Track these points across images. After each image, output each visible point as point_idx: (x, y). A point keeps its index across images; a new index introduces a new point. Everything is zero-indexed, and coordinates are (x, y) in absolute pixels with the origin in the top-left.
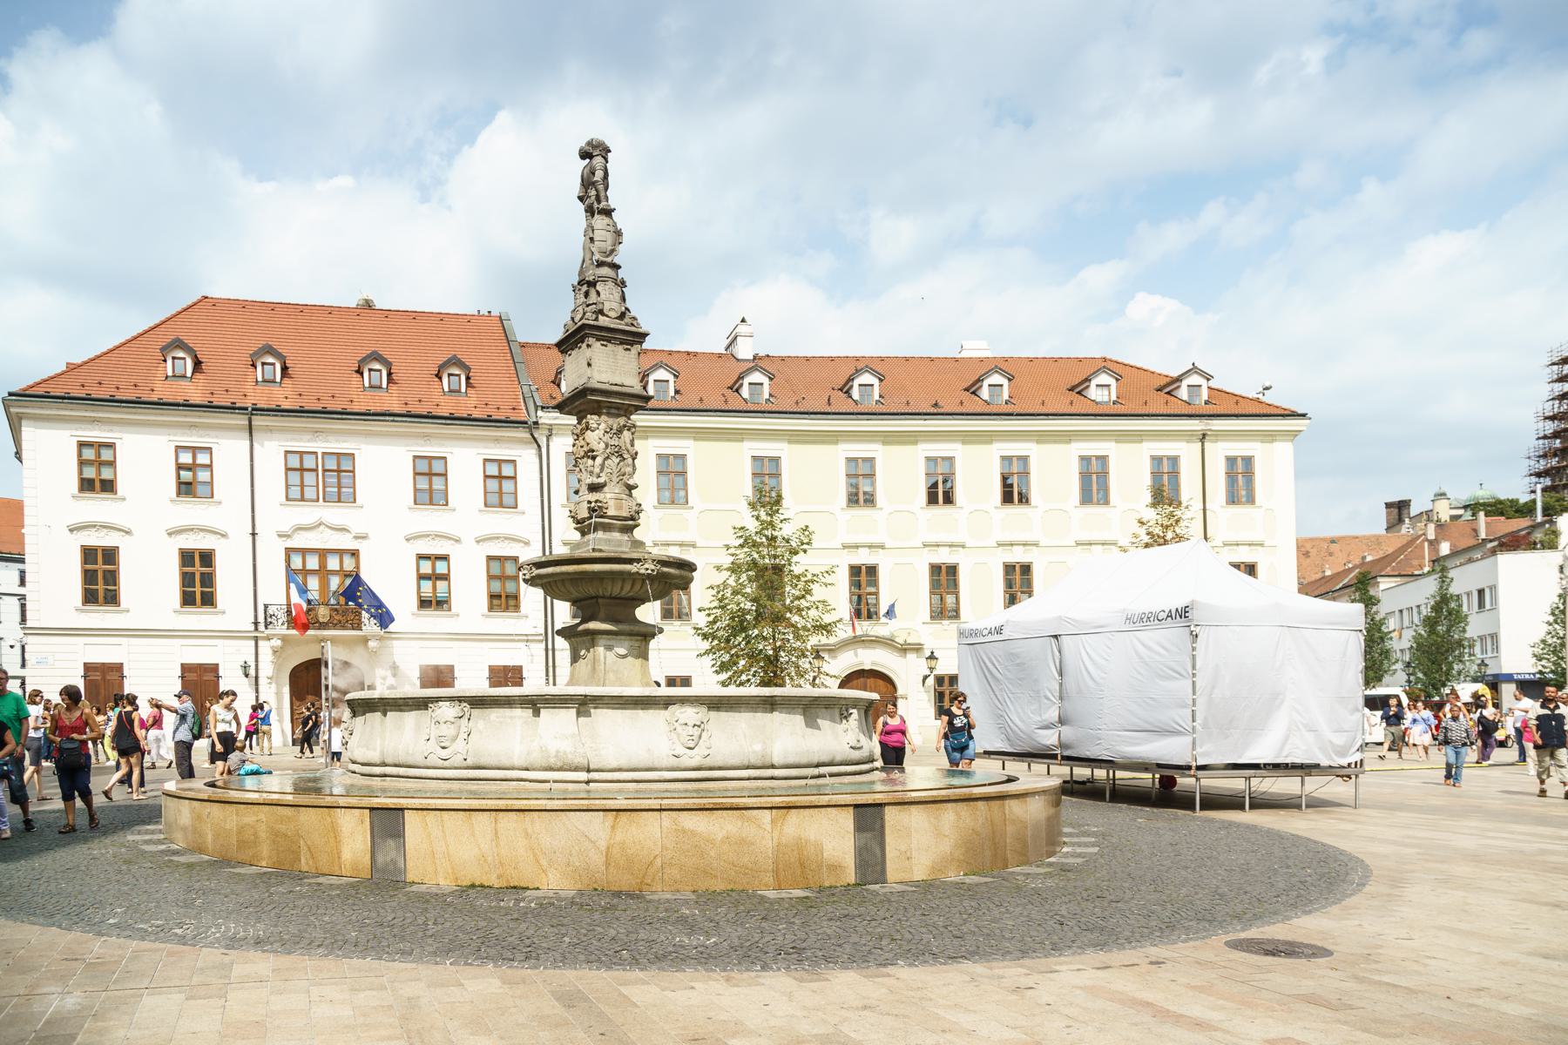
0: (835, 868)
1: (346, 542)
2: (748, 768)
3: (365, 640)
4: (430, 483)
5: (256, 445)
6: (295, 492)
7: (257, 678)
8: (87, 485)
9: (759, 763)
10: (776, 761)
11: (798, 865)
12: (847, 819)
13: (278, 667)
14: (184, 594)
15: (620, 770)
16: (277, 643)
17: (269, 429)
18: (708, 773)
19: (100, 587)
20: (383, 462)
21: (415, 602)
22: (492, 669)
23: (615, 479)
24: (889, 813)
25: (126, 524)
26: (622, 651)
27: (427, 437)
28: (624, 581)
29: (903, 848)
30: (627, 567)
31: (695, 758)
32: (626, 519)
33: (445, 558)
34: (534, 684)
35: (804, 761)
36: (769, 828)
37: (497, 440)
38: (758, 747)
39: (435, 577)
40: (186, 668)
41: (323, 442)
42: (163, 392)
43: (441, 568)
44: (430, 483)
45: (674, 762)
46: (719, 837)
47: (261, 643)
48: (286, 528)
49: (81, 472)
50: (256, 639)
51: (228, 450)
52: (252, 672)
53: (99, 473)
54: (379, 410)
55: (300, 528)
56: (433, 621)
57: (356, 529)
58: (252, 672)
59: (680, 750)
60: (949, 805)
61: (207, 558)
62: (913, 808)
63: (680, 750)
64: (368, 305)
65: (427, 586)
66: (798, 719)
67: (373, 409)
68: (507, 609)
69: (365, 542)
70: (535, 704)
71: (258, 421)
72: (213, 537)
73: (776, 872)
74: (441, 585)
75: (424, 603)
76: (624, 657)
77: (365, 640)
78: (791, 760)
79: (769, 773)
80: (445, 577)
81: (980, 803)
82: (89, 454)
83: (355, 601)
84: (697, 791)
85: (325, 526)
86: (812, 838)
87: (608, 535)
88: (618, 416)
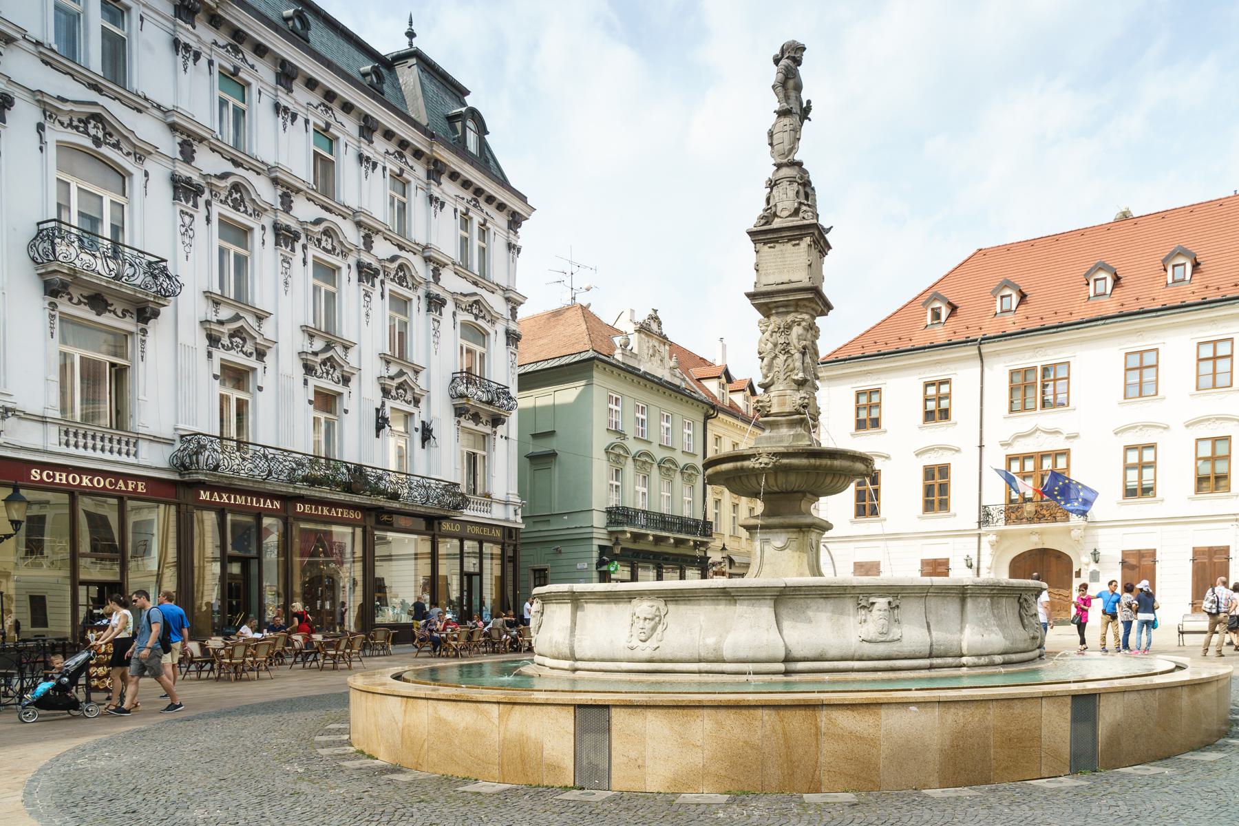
0: (554, 768)
1: (1057, 444)
2: (700, 661)
3: (1069, 530)
4: (1141, 376)
5: (986, 369)
6: (1018, 404)
7: (978, 569)
8: (929, 416)
9: (711, 656)
10: (727, 654)
11: (519, 757)
12: (567, 720)
13: (997, 558)
14: (858, 507)
15: (593, 660)
16: (993, 538)
17: (997, 354)
18: (658, 666)
19: (936, 498)
20: (1094, 364)
21: (1120, 491)
22: (925, 563)
23: (782, 377)
24: (617, 716)
25: (956, 444)
26: (779, 544)
27: (1139, 332)
28: (756, 476)
29: (633, 755)
30: (746, 463)
31: (646, 650)
32: (791, 414)
33: (1152, 446)
34: (960, 575)
35: (762, 654)
36: (496, 721)
37: (1213, 321)
38: (711, 641)
39: (1142, 466)
40: (1197, 552)
41: (1033, 356)
42: (919, 340)
43: (1148, 456)
44: (1141, 376)
45: (629, 654)
46: (462, 725)
47: (983, 539)
48: (1006, 437)
49: (858, 415)
50: (979, 536)
51: (963, 377)
52: (975, 564)
53: (870, 413)
54: (1094, 316)
55: (1018, 436)
56: (1140, 508)
57: (1068, 430)
58: (975, 564)
59: (635, 642)
60: (706, 712)
61: (944, 470)
62: (650, 714)
63: (635, 642)
64: (1125, 216)
65: (1133, 475)
66: (765, 612)
67: (1087, 317)
68: (1217, 489)
69: (1075, 441)
70: (962, 593)
71: (986, 349)
72: (949, 453)
73: (501, 765)
74: (1148, 473)
75: (1130, 493)
76: (782, 549)
77: (1069, 530)
78: (742, 654)
79: (704, 666)
80: (1152, 465)
81: (759, 712)
82: (932, 391)
83: (1059, 493)
84: (700, 684)
85: (1039, 431)
86: (533, 735)
87: (774, 433)
88: (788, 313)
